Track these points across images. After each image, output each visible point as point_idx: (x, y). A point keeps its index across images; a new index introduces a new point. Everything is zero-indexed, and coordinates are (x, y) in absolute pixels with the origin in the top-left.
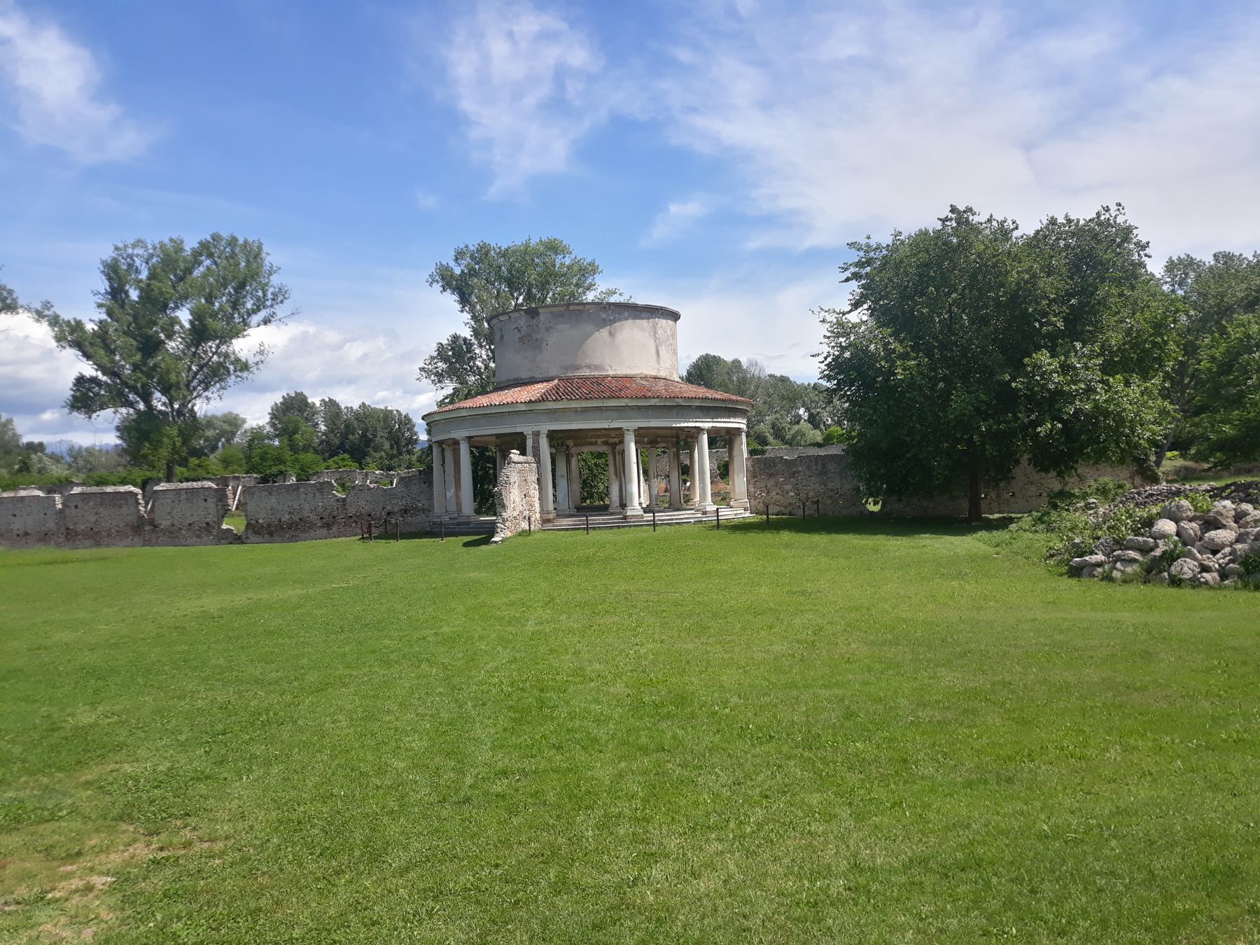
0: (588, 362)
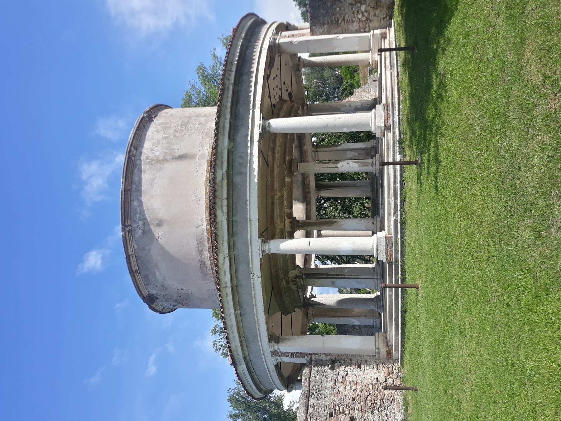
0: (195, 253)
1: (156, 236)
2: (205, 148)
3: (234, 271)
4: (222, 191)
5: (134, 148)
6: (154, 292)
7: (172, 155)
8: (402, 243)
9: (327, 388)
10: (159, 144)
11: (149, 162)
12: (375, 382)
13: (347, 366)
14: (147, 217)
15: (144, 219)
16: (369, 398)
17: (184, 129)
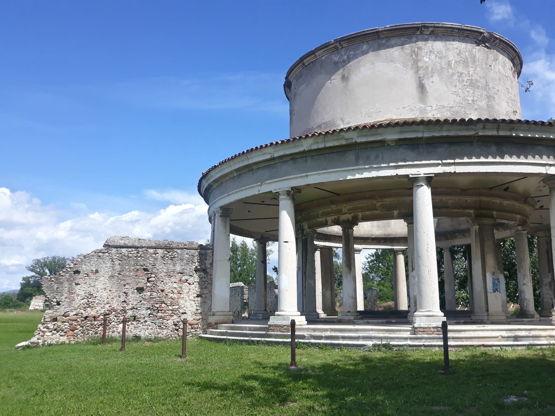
1: (333, 77)
2: (435, 112)
4: (334, 140)
5: (432, 31)
7: (424, 77)
9: (174, 265)
10: (440, 58)
11: (414, 51)
12: (181, 311)
13: (199, 284)
14: (351, 63)
15: (349, 60)
16: (163, 305)
17: (465, 83)
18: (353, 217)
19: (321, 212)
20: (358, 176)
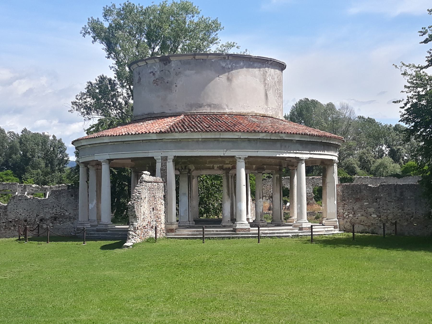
0: (208, 101)
1: (221, 76)
2: (270, 111)
3: (228, 140)
6: (173, 64)
8: (250, 237)
14: (233, 71)
18: (232, 167)
19: (208, 160)
20: (281, 155)
